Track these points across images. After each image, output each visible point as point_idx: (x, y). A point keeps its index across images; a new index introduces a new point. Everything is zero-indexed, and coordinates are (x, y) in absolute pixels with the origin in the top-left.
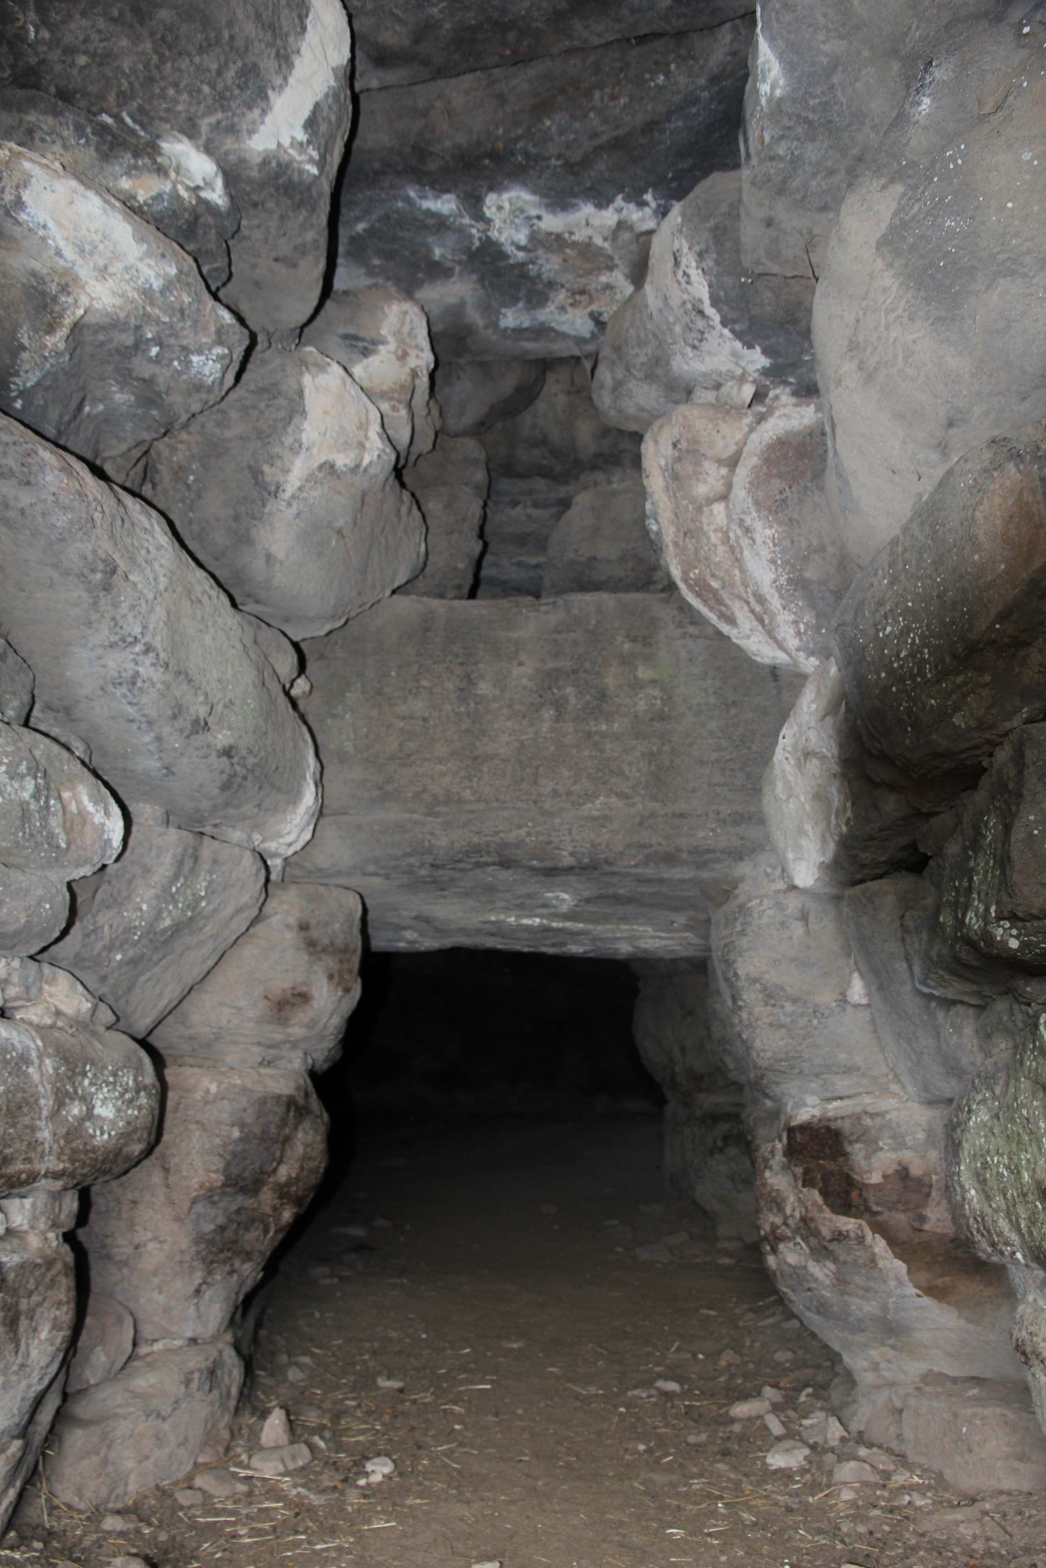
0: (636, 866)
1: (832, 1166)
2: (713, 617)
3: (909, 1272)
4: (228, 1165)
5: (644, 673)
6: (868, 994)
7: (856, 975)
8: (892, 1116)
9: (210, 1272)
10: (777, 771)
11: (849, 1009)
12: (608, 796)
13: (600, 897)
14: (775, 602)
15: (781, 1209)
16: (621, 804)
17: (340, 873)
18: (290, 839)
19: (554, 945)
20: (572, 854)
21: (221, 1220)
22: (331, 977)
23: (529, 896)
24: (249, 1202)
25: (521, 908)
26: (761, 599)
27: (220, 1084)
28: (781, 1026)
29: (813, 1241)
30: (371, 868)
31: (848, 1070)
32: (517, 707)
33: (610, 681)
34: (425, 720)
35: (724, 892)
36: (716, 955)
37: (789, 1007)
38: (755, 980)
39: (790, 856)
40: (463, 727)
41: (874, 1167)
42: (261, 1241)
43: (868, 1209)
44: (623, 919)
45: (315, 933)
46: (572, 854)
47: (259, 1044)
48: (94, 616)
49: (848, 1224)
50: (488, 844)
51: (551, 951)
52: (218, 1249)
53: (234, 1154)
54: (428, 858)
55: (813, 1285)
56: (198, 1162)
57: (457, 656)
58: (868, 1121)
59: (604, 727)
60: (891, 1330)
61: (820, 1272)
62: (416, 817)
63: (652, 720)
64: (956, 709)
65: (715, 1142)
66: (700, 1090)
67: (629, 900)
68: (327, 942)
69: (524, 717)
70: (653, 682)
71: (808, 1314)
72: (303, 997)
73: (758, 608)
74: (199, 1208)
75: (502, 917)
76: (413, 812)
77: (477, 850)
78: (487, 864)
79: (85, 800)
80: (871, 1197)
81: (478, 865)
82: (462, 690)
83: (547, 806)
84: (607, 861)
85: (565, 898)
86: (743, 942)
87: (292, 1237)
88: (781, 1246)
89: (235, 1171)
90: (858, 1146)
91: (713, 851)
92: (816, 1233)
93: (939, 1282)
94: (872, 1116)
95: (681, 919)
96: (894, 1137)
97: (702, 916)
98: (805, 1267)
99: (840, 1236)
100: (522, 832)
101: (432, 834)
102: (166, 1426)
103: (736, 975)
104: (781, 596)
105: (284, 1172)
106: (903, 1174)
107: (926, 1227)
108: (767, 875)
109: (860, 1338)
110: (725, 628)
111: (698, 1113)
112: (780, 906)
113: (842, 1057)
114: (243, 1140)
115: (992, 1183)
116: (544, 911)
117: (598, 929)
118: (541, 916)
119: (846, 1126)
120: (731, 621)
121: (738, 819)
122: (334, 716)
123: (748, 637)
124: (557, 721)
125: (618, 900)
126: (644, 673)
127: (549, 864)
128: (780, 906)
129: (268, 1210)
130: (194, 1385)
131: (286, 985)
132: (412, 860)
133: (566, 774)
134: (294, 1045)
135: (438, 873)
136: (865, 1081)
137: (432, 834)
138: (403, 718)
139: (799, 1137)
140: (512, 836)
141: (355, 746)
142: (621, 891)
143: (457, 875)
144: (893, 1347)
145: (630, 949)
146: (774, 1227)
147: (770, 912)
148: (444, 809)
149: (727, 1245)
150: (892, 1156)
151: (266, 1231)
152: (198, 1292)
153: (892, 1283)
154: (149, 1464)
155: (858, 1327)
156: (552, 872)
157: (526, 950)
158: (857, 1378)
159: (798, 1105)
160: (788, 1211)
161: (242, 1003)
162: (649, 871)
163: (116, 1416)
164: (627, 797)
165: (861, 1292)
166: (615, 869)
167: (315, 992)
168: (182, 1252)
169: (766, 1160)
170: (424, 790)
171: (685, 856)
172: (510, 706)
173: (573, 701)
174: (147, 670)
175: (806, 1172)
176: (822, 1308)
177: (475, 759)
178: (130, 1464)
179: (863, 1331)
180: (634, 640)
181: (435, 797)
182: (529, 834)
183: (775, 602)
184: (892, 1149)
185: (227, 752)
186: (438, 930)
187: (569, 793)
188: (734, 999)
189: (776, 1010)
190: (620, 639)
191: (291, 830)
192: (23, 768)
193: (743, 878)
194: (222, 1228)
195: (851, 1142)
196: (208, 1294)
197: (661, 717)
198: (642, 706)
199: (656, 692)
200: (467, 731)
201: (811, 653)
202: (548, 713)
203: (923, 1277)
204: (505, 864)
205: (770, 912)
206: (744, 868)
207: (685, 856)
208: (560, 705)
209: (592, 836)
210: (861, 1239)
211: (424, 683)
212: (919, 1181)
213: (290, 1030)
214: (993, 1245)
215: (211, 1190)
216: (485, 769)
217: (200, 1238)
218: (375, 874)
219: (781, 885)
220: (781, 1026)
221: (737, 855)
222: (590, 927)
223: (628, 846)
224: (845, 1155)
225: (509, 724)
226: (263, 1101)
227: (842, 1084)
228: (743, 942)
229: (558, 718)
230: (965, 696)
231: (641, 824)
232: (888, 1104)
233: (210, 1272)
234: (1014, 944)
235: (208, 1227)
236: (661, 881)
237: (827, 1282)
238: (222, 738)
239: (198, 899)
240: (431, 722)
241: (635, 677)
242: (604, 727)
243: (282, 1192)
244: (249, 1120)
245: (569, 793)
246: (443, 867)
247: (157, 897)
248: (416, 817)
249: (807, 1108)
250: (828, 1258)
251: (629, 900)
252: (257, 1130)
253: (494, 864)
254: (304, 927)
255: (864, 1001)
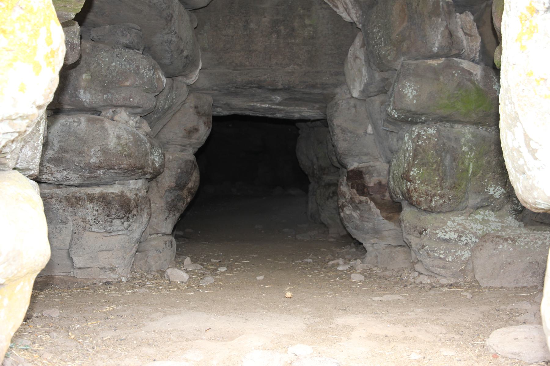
0: (303, 89)
1: (359, 182)
2: (331, 5)
3: (381, 212)
4: (176, 181)
5: (307, 22)
6: (373, 131)
7: (370, 125)
8: (378, 167)
9: (169, 213)
10: (349, 60)
11: (368, 135)
12: (294, 65)
13: (290, 98)
14: (350, 6)
15: (345, 197)
16: (298, 68)
17: (204, 89)
18: (193, 79)
19: (271, 114)
20: (282, 84)
21: (173, 198)
22: (205, 123)
23: (266, 97)
24: (181, 193)
25: (262, 101)
26: (346, 4)
27: (172, 156)
28: (346, 140)
29: (353, 204)
30: (215, 88)
31: (366, 154)
32: (264, 33)
33: (296, 24)
34: (232, 37)
35: (332, 97)
36: (328, 118)
37: (349, 134)
38: (339, 126)
39: (352, 87)
40: (246, 40)
41: (371, 182)
42: (182, 206)
43: (369, 194)
44: (297, 105)
45: (200, 109)
46: (282, 84)
47: (181, 145)
48: (166, 27)
49: (363, 198)
50: (254, 80)
51: (270, 116)
52: (172, 207)
53: (179, 177)
54: (235, 85)
55: (354, 220)
56: (167, 179)
57: (243, 13)
58: (370, 168)
59: (293, 41)
60: (376, 232)
61: (355, 214)
62: (230, 71)
63: (309, 39)
64: (389, 55)
65: (329, 194)
66: (324, 174)
67: (300, 100)
68: (203, 112)
69: (266, 36)
70: (310, 25)
71: (353, 230)
72: (196, 130)
73: (345, 6)
74: (167, 194)
75: (255, 104)
76: (229, 69)
77: (251, 82)
78: (254, 87)
79: (160, 74)
80: (370, 190)
81: (251, 87)
82: (245, 26)
83: (274, 68)
84: (293, 87)
85: (278, 98)
86: (336, 114)
87: (190, 206)
88: (345, 209)
89: (179, 182)
90: (367, 175)
91: (328, 84)
92: (354, 202)
93: (389, 215)
94: (372, 167)
95: (317, 106)
96: (378, 173)
97: (324, 105)
98: (351, 214)
99: (361, 202)
100: (266, 77)
101: (236, 77)
102: (161, 255)
103: (333, 124)
104: (352, 5)
105: (190, 185)
106: (380, 183)
107: (385, 198)
108: (345, 93)
109: (367, 236)
110: (335, 9)
111: (323, 184)
112: (348, 103)
113: (365, 150)
114: (182, 173)
115: (395, 179)
116: (270, 102)
117: (288, 109)
118: (269, 104)
119: (364, 170)
120: (337, 7)
121: (337, 74)
122: (201, 34)
123: (342, 13)
124: (278, 38)
125: (296, 99)
126: (307, 22)
127: (274, 88)
128: (348, 103)
129: (185, 196)
130: (167, 245)
131: (191, 126)
132: (229, 86)
133: (280, 57)
134: (190, 145)
135: (236, 90)
136: (372, 157)
137: (236, 77)
138: (225, 36)
139: (350, 174)
140: (262, 78)
141: (208, 45)
142: (297, 96)
143: (243, 90)
144: (377, 238)
145: (299, 116)
146: (343, 203)
147: (345, 105)
148: (239, 68)
149: (333, 235)
150: (377, 178)
151: (184, 204)
152: (166, 219)
153: (376, 216)
154: (157, 264)
155: (367, 233)
156: (275, 90)
157: (261, 115)
158: (367, 249)
159: (351, 165)
160: (347, 197)
161: (177, 131)
162: (307, 90)
163: (148, 250)
164: (300, 65)
165: (367, 220)
166: (296, 90)
167: (200, 128)
168: (162, 207)
169: (341, 183)
170: (233, 62)
171: (319, 86)
172: (262, 33)
173: (283, 31)
174: (174, 39)
175: (352, 184)
176: (357, 228)
177: (250, 51)
178: (153, 263)
179: (368, 233)
180: (304, 9)
181: (236, 64)
182: (268, 77)
183: (350, 6)
184: (377, 176)
185: (187, 57)
186: (231, 108)
187: (281, 64)
188: (333, 132)
189: (345, 135)
190: (299, 8)
191: (194, 77)
192: (151, 68)
193: (337, 94)
194: (173, 200)
195: (365, 174)
196: (168, 221)
197: (313, 38)
198: (306, 34)
199: (311, 29)
200: (247, 41)
201: (360, 23)
202: (275, 36)
203: (385, 214)
204: (260, 87)
205: (345, 105)
206: (338, 90)
207: (319, 86)
208: (278, 33)
209: (289, 78)
210: (367, 202)
211: (232, 23)
212: (384, 185)
213: (192, 140)
214: (395, 195)
215: (171, 188)
216: (253, 55)
217: (167, 203)
218: (216, 90)
219: (349, 96)
220: (346, 140)
221: (336, 86)
222: (285, 108)
223: (300, 82)
224: (363, 178)
225: (261, 39)
226: (186, 161)
227: (364, 158)
228: (336, 114)
229: (278, 38)
230: (391, 52)
231: (305, 75)
232: (378, 164)
233: (169, 213)
234: (396, 116)
235: (170, 200)
236: (311, 94)
237: (358, 218)
238: (185, 53)
239: (173, 99)
240: (234, 38)
241: (304, 23)
242: (293, 41)
243: (189, 190)
244: (183, 167)
245: (281, 64)
246: (239, 88)
247: (165, 99)
248: (230, 71)
249: (353, 165)
250: (357, 209)
251: (300, 100)
252: (185, 170)
253: (256, 87)
254: (196, 107)
255: (372, 133)
